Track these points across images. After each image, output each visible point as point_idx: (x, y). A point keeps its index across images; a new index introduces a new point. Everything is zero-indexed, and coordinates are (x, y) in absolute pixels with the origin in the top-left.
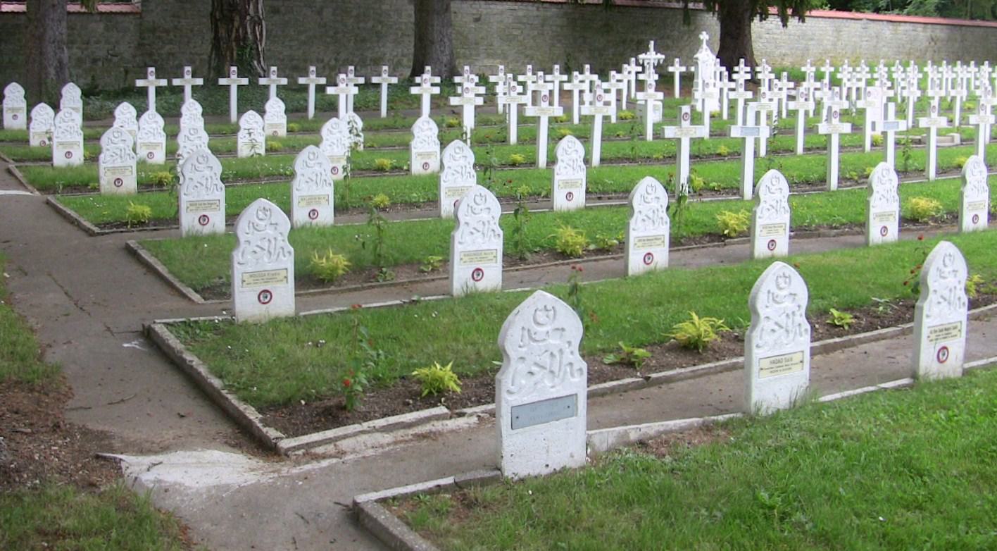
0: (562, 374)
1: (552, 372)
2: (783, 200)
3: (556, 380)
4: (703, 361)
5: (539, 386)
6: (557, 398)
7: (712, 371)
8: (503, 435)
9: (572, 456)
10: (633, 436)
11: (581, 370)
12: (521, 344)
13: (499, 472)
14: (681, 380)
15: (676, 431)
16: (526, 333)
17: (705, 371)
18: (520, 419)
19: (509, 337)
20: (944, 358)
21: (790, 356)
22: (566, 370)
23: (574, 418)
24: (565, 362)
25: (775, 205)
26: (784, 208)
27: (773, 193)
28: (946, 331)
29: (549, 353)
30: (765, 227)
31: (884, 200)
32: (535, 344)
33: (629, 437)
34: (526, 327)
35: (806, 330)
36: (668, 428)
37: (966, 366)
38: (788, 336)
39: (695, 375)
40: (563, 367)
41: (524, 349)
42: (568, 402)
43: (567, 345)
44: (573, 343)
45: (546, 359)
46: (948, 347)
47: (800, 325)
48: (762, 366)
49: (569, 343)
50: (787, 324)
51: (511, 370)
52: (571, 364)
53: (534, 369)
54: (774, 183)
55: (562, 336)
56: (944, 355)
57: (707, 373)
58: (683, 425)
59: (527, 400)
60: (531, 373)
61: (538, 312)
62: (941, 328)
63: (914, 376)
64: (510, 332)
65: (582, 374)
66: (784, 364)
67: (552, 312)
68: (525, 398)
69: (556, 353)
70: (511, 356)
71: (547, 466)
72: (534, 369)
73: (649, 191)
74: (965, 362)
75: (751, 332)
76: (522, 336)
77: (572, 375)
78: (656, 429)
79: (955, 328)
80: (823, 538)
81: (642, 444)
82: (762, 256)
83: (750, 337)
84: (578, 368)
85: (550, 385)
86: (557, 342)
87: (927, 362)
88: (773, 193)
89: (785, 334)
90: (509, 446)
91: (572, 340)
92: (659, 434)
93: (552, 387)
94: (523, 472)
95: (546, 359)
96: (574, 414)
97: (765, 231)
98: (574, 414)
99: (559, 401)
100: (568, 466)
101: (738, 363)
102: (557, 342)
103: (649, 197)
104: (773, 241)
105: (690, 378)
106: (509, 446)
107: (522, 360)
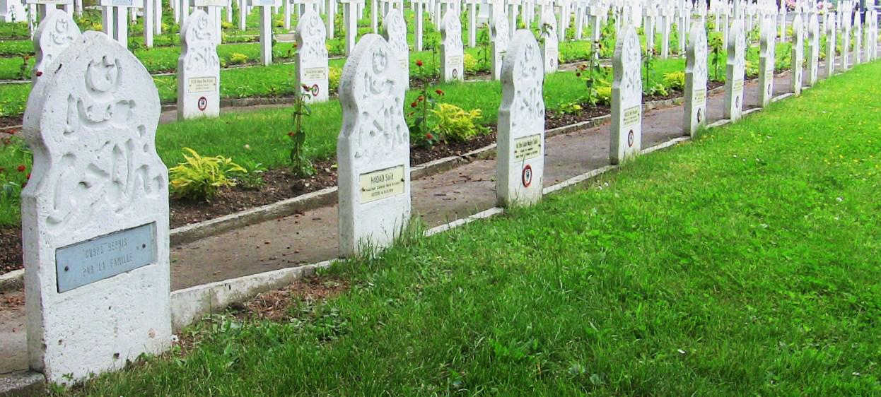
0: (131, 186)
1: (117, 182)
2: (212, 48)
3: (126, 198)
4: (216, 213)
5: (98, 209)
6: (127, 230)
7: (236, 223)
8: (46, 305)
9: (152, 335)
10: (223, 298)
11: (159, 178)
12: (69, 128)
13: (41, 377)
14: (201, 237)
15: (273, 287)
16: (74, 106)
17: (228, 224)
18: (70, 268)
19: (47, 114)
20: (529, 182)
21: (390, 171)
22: (137, 178)
23: (152, 265)
24: (137, 164)
25: (203, 55)
26: (213, 57)
27: (201, 39)
28: (527, 145)
29: (110, 147)
30: (194, 80)
31: (313, 53)
32: (90, 129)
33: (216, 300)
34: (76, 96)
35: (405, 135)
36: (263, 283)
37: (545, 191)
38: (387, 142)
39: (218, 231)
40: (133, 173)
41: (73, 138)
42: (143, 236)
43: (138, 133)
44: (147, 130)
45: (106, 159)
46: (531, 166)
47: (398, 127)
48: (402, 168)
49: (141, 128)
50: (385, 124)
51: (53, 177)
52: (144, 167)
53: (90, 176)
54: (202, 26)
55: (130, 114)
56: (528, 176)
57: (232, 226)
58: (280, 277)
59: (81, 235)
60: (84, 184)
61: (93, 68)
62: (525, 140)
63: (502, 203)
64: (48, 105)
65: (160, 186)
66: (385, 183)
67: (115, 69)
68: (77, 232)
69: (122, 147)
70: (51, 151)
71: (117, 355)
72: (90, 176)
73: (60, 28)
74: (544, 187)
75: (347, 134)
76: (70, 112)
77: (147, 189)
78: (249, 284)
79: (536, 142)
80: (736, 378)
81: (236, 308)
82: (192, 117)
83: (346, 144)
84: (157, 175)
85: (116, 206)
86: (124, 126)
87: (515, 189)
88: (201, 39)
89: (384, 139)
90: (54, 325)
91: (146, 124)
92: (256, 290)
93: (118, 210)
94: (81, 374)
95: (107, 155)
96: (153, 260)
97: (194, 86)
98: (153, 260)
99: (128, 235)
100: (97, 373)
101: (264, 212)
102: (124, 126)
103: (60, 36)
104: (203, 98)
105: (212, 234)
106: (54, 325)
107: (68, 160)
